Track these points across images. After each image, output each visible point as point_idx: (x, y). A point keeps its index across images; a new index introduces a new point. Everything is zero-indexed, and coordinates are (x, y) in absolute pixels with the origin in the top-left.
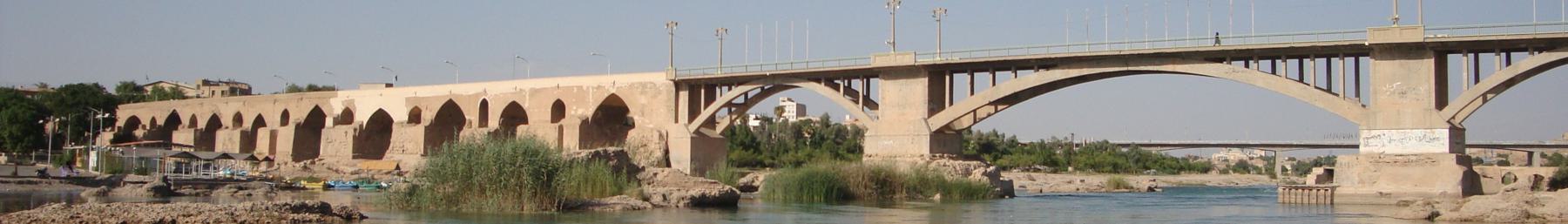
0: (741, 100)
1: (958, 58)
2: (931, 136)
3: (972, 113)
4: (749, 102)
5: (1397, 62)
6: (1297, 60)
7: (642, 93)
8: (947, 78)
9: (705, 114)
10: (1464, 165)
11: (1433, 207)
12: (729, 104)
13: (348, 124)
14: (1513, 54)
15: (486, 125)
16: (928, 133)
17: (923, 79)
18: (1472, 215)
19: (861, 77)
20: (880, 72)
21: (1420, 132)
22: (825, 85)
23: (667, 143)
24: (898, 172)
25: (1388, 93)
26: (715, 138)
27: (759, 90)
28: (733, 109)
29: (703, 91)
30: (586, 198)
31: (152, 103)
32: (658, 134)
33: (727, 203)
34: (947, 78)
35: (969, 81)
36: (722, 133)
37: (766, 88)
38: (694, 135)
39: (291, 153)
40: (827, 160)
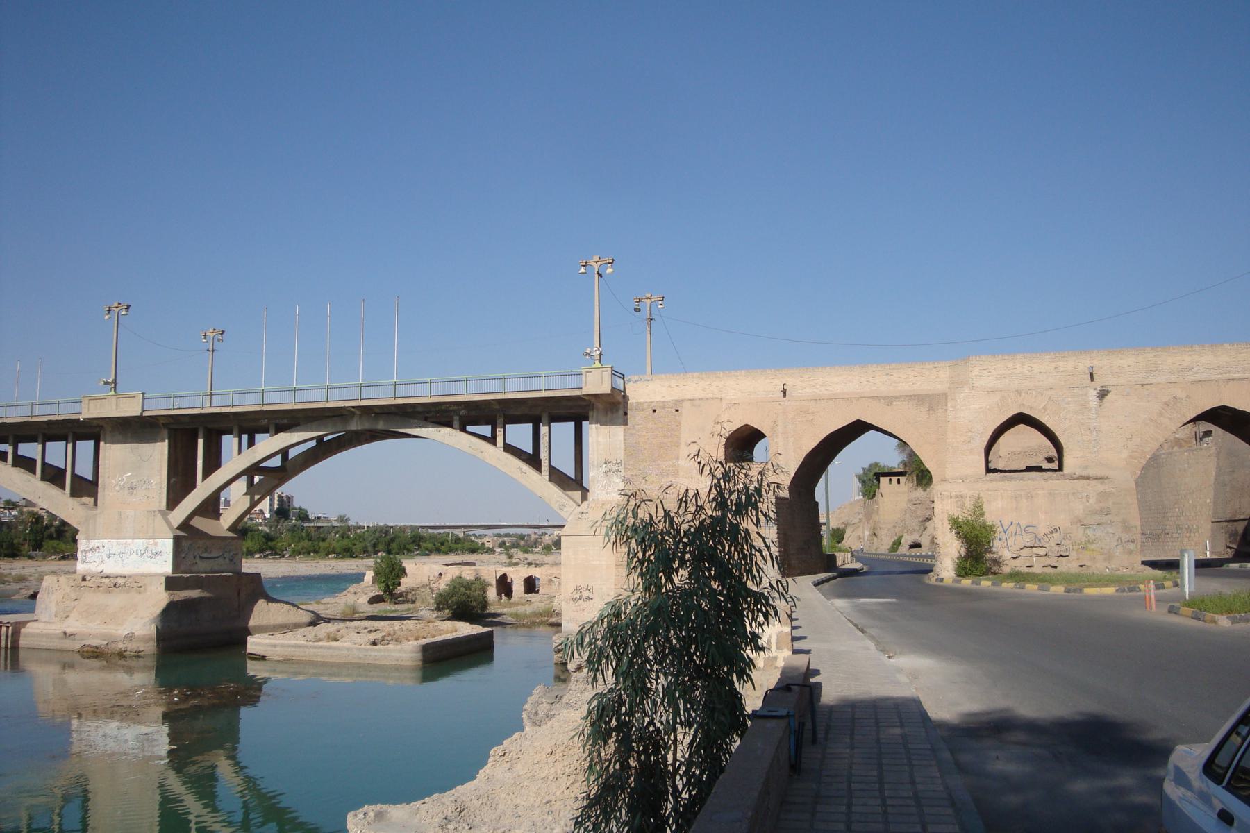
0: (276, 462)
3: (279, 457)
4: (289, 467)
5: (128, 445)
6: (572, 425)
9: (203, 489)
12: (254, 469)
14: (258, 436)
19: (236, 431)
21: (140, 544)
25: (117, 488)
27: (313, 443)
28: (257, 479)
29: (201, 442)
35: (548, 430)
36: (233, 528)
37: (326, 439)
38: (181, 533)
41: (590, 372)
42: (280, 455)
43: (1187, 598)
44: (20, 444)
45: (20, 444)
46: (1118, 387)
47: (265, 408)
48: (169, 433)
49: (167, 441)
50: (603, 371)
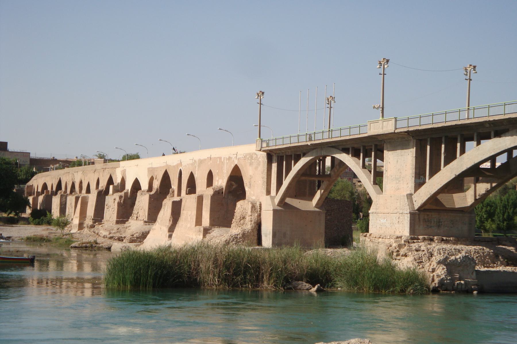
2: (413, 215)
3: (505, 155)
8: (459, 145)
10: (52, 197)
11: (94, 232)
13: (200, 226)
15: (174, 203)
17: (412, 149)
18: (32, 234)
22: (352, 156)
23: (260, 215)
24: (148, 250)
31: (75, 168)
32: (250, 206)
33: (263, 97)
34: (459, 145)
40: (385, 257)
41: (378, 122)
42: (378, 160)
43: (38, 208)
46: (111, 167)
49: (415, 148)
50: (383, 121)
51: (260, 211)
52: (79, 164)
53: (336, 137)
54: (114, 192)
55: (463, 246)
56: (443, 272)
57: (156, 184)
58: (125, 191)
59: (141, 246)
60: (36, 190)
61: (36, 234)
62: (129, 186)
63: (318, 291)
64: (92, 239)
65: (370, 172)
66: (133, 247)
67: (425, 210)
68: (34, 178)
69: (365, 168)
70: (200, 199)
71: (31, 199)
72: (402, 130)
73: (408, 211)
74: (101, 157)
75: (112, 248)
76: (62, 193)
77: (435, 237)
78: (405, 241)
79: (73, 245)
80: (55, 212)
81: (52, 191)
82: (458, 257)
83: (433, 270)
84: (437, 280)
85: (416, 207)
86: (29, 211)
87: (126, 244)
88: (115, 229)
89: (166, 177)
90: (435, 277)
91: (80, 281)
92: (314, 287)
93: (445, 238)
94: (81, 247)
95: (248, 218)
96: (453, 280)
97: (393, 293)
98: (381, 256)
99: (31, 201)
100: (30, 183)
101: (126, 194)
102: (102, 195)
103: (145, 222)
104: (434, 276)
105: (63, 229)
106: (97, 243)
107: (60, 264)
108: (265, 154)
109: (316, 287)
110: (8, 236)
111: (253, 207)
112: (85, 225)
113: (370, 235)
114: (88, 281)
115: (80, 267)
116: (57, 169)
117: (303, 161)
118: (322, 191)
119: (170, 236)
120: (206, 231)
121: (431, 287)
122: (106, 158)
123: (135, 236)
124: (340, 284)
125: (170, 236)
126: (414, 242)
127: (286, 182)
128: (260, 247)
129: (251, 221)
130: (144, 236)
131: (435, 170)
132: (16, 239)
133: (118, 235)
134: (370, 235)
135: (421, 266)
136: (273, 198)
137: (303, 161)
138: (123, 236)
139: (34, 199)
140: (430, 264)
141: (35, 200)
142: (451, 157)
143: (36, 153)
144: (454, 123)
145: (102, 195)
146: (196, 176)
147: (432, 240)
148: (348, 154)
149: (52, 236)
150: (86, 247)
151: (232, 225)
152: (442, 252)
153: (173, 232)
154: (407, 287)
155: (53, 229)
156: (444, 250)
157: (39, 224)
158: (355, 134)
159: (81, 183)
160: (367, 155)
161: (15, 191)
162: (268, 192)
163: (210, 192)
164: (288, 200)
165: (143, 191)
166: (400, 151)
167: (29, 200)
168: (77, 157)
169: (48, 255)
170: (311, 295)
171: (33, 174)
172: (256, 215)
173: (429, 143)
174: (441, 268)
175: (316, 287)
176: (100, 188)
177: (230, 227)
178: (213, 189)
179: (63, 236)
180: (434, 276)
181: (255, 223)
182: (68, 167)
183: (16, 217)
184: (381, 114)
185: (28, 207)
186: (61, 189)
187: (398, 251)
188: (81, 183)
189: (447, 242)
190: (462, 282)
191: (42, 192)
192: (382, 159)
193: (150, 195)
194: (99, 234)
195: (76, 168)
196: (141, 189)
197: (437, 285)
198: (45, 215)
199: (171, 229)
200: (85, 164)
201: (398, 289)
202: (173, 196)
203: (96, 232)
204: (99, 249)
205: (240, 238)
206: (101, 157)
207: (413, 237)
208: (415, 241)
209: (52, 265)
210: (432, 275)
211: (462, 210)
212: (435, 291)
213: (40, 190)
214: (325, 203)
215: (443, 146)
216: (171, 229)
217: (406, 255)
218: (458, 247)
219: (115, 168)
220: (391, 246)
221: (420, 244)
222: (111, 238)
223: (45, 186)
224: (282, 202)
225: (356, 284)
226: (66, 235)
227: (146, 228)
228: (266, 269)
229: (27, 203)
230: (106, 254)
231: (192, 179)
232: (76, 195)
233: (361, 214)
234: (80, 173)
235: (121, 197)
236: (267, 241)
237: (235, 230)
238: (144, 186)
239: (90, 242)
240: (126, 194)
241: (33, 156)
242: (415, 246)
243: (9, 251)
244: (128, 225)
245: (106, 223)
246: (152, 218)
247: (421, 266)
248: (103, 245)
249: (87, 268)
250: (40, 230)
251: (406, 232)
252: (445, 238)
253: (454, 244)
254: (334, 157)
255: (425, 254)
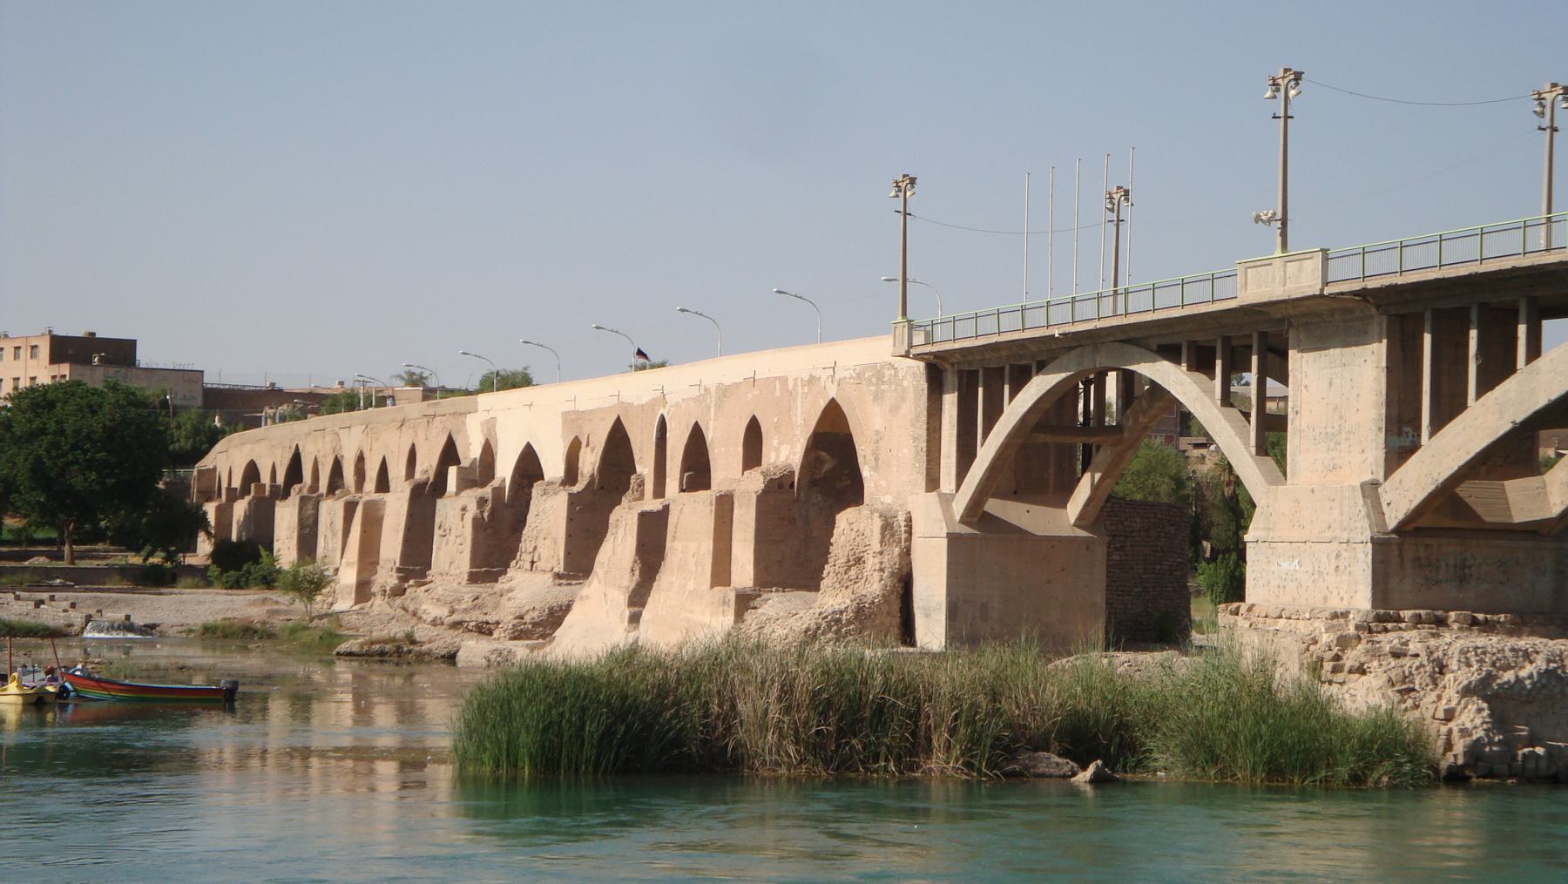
1: (878, 423)
2: (1381, 547)
7: (876, 398)
8: (1522, 330)
15: (644, 516)
16: (1364, 532)
17: (1376, 345)
20: (1286, 322)
22: (1190, 369)
26: (1060, 539)
30: (1277, 676)
32: (877, 524)
34: (1522, 330)
39: (1233, 433)
41: (1270, 264)
43: (234, 537)
44: (1545, 323)
45: (1545, 323)
47: (1372, 284)
48: (1389, 323)
51: (909, 539)
52: (348, 402)
53: (1141, 310)
54: (461, 488)
55: (1537, 640)
56: (1478, 721)
57: (590, 462)
58: (495, 483)
59: (548, 649)
60: (224, 485)
61: (229, 615)
62: (505, 469)
63: (1096, 781)
64: (397, 630)
65: (1247, 415)
66: (521, 651)
67: (1419, 532)
68: (218, 447)
69: (1232, 405)
70: (725, 505)
71: (210, 509)
72: (1345, 287)
73: (1367, 535)
74: (414, 380)
75: (461, 656)
76: (305, 492)
77: (1452, 614)
78: (1357, 627)
79: (343, 647)
80: (285, 549)
81: (274, 486)
82: (1523, 673)
83: (1449, 715)
84: (1459, 746)
85: (1392, 523)
86: (205, 546)
87: (500, 642)
88: (468, 598)
89: (618, 441)
90: (1456, 735)
91: (364, 754)
92: (1084, 768)
93: (1480, 616)
94: (368, 654)
95: (871, 562)
96: (1510, 744)
97: (1328, 789)
98: (1289, 673)
99: (211, 518)
100: (207, 462)
101: (498, 491)
102: (426, 496)
103: (558, 576)
104: (1450, 731)
105: (311, 599)
106: (413, 642)
107: (303, 701)
108: (922, 365)
109: (1091, 769)
110: (148, 621)
111: (887, 527)
112: (375, 588)
113: (1250, 609)
114: (386, 754)
115: (363, 712)
116: (283, 419)
117: (1039, 386)
118: (1098, 476)
119: (635, 619)
120: (744, 602)
121: (1444, 765)
122: (432, 383)
123: (527, 618)
124: (1161, 759)
125: (635, 619)
126: (1386, 630)
127: (986, 452)
128: (911, 650)
129: (882, 570)
130: (555, 618)
131: (1449, 407)
132: (172, 632)
133: (476, 616)
134: (1250, 609)
135: (1409, 703)
136: (946, 501)
137: (1039, 386)
138: (492, 618)
139: (219, 509)
140: (1439, 697)
141: (224, 513)
142: (1497, 369)
143: (224, 372)
144: (1507, 264)
145: (426, 496)
146: (709, 436)
147: (1441, 622)
148: (1177, 361)
149: (278, 622)
150: (382, 653)
151: (823, 584)
152: (1473, 660)
153: (643, 605)
154: (1370, 767)
155: (281, 599)
156: (1481, 652)
157: (237, 585)
158: (1199, 301)
159: (361, 459)
160: (1236, 365)
161: (161, 486)
162: (933, 483)
163: (755, 482)
164: (994, 506)
165: (550, 483)
166: (1338, 350)
167: (205, 514)
168: (341, 383)
169: (267, 679)
170: (1075, 792)
171: (214, 437)
172: (897, 550)
173: (1428, 326)
174: (1473, 708)
175: (1091, 769)
176: (418, 476)
177: (817, 589)
178: (764, 474)
179: (312, 620)
180: (1450, 731)
181: (892, 574)
182: (317, 412)
183: (168, 565)
184: (1279, 239)
185: (202, 537)
186: (300, 480)
187: (1337, 658)
188: (361, 459)
189: (1488, 627)
190: (1540, 750)
191: (245, 490)
192: (1284, 379)
193: (570, 495)
194: (420, 613)
195: (343, 417)
196: (542, 477)
197: (1460, 761)
198: (256, 558)
199: (638, 598)
200: (368, 405)
201: (1343, 772)
202: (642, 497)
203: (411, 608)
204: (422, 658)
205: (849, 622)
206: (414, 380)
207: (1385, 614)
208: (1390, 626)
209: (278, 709)
210: (1444, 729)
211: (1534, 531)
212: (1456, 778)
213: (236, 483)
214: (1103, 512)
215: (1473, 333)
216: (638, 598)
217: (1361, 671)
218: (1524, 643)
219: (464, 414)
220: (1316, 642)
221: (1406, 635)
222: (456, 625)
223: (252, 472)
224: (975, 513)
225: (1214, 759)
226: (321, 617)
227: (561, 594)
228: (939, 713)
229: (201, 522)
230: (441, 673)
231: (697, 445)
232: (348, 498)
233: (1207, 545)
234: (357, 431)
235: (482, 502)
236: (931, 631)
237: (833, 598)
238: (553, 467)
239: (393, 640)
240: (498, 491)
241: (210, 380)
242: (1388, 641)
243: (157, 668)
244: (506, 586)
245: (438, 580)
246: (579, 563)
247: (1409, 703)
248: (433, 646)
249: (384, 715)
250: (243, 605)
251: (1359, 599)
252: (1480, 616)
253: (1511, 633)
254: (1133, 372)
255: (1422, 665)
